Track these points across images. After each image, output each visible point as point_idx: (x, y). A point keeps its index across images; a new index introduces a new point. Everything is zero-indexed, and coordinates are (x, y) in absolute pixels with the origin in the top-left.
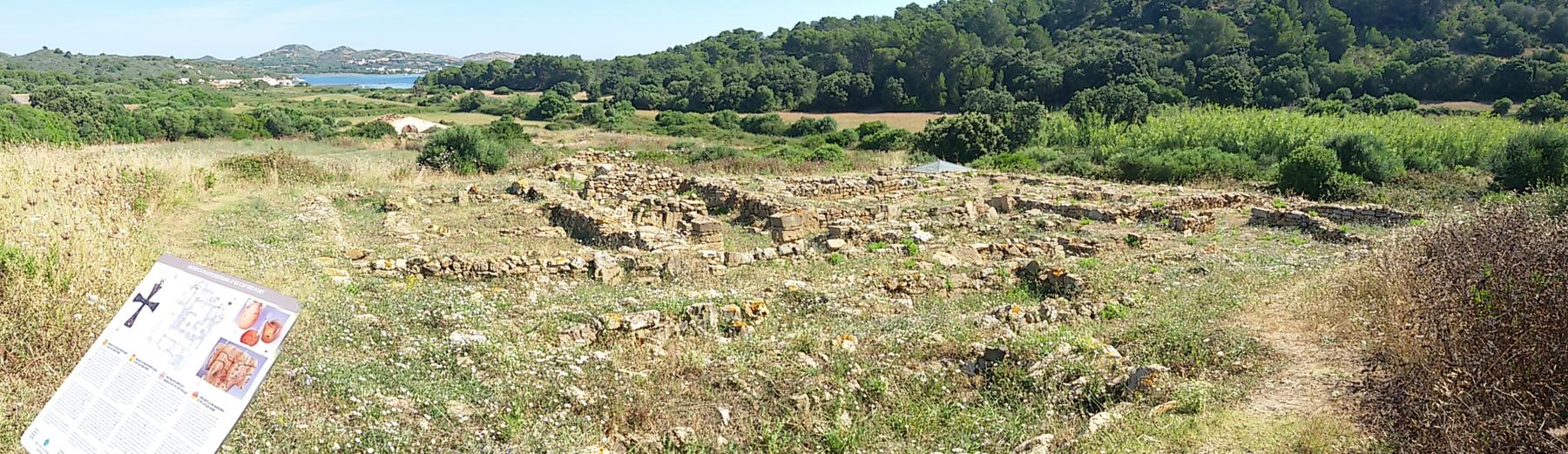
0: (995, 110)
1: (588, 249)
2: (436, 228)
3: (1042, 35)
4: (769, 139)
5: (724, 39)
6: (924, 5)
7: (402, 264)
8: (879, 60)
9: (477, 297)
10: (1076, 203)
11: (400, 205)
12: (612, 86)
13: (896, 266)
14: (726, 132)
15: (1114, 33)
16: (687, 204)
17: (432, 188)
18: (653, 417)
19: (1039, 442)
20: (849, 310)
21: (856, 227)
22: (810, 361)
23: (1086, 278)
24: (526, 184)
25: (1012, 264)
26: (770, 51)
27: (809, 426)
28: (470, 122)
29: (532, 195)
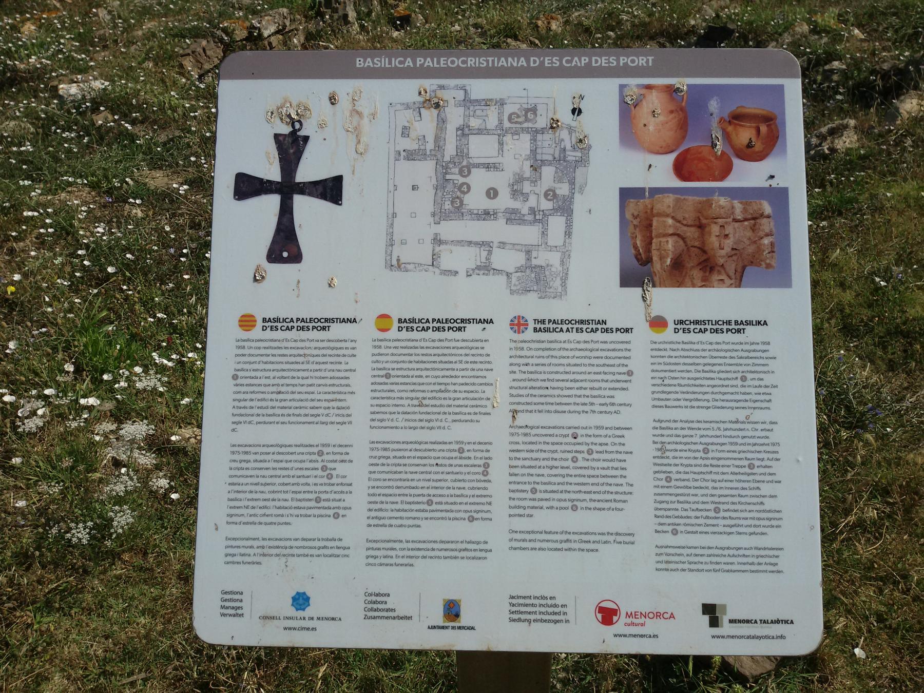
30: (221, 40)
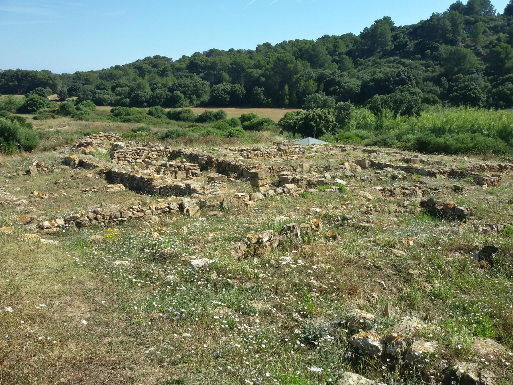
3: (348, 62)
6: (273, 44)
8: (249, 76)
14: (158, 120)
15: (395, 60)
26: (179, 70)
30: (246, 243)
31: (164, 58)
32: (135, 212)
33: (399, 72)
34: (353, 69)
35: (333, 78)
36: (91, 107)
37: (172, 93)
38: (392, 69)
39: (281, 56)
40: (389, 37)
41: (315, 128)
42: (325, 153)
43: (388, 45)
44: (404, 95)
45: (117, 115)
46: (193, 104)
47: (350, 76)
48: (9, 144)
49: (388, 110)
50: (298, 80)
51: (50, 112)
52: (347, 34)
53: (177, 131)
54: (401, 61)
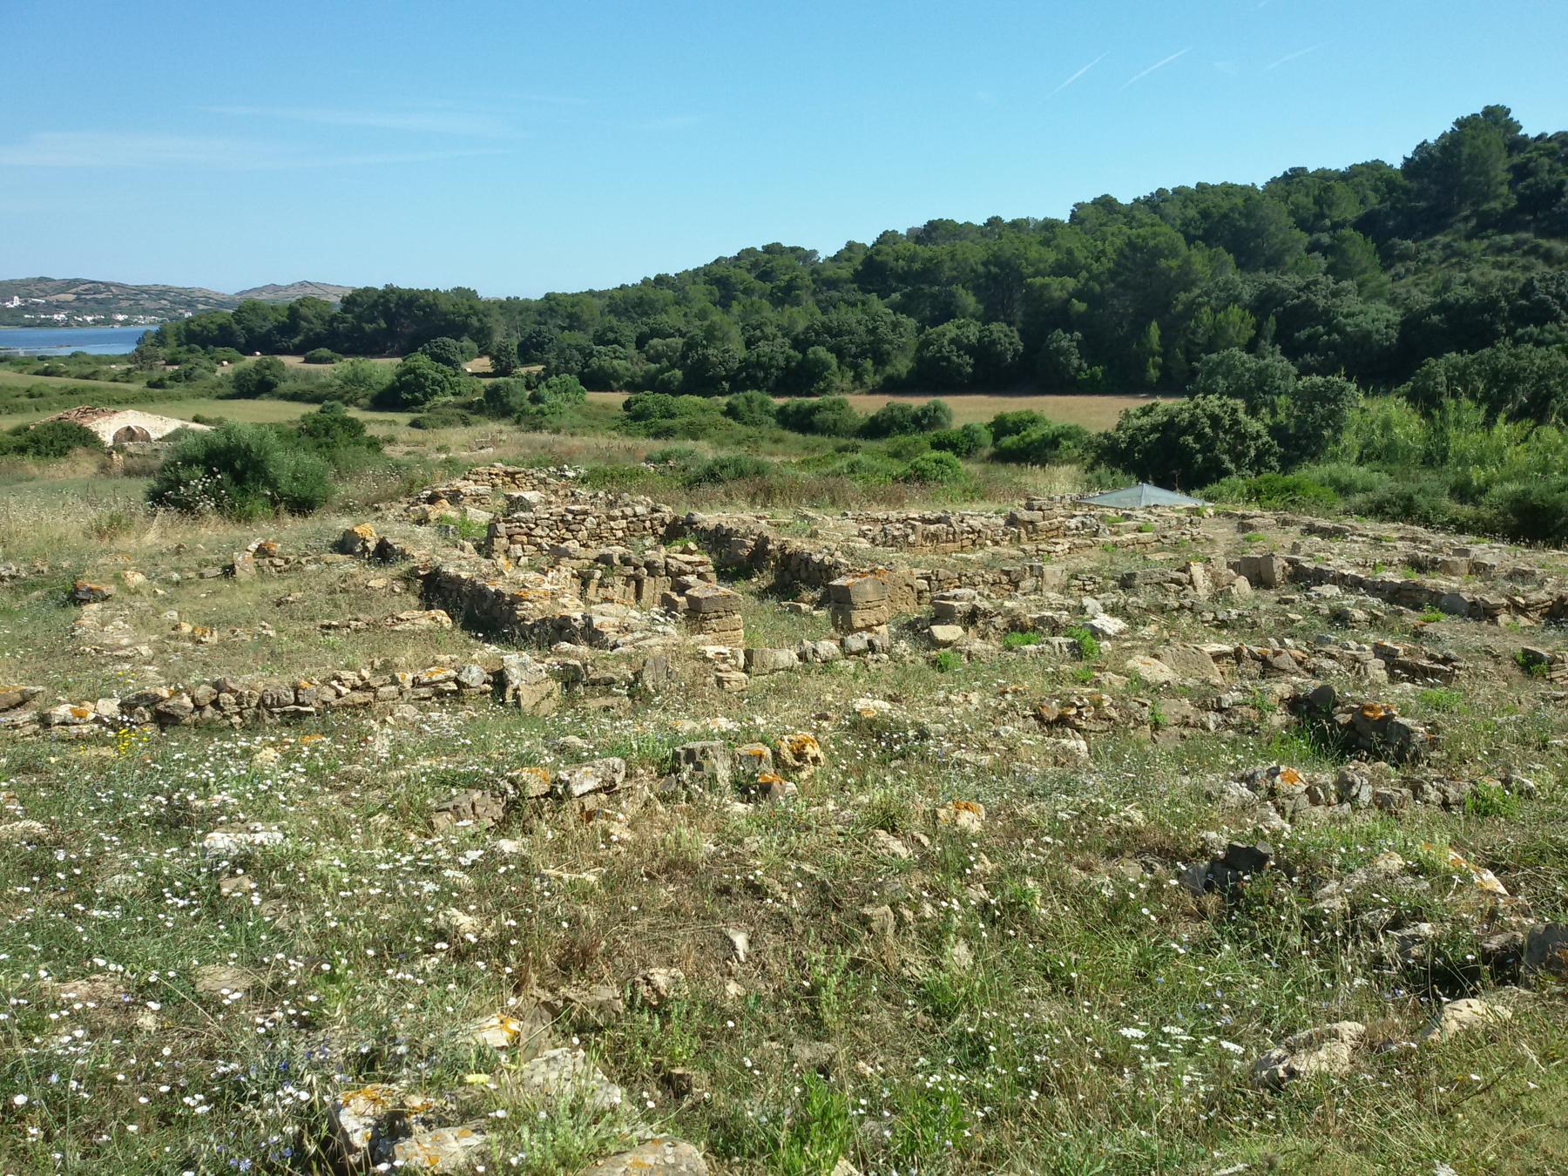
0: (1255, 391)
1: (492, 649)
2: (187, 628)
3: (1361, 249)
4: (828, 443)
5: (745, 263)
6: (1125, 198)
7: (109, 707)
8: (1036, 298)
9: (268, 756)
10: (1416, 578)
11: (110, 589)
12: (540, 346)
13: (1056, 678)
14: (751, 430)
15: (1518, 244)
16: (679, 559)
17: (178, 551)
18: (607, 955)
19: (1335, 1035)
20: (970, 757)
21: (984, 605)
22: (897, 846)
23: (1434, 728)
24: (369, 531)
25: (1281, 689)
26: (832, 284)
27: (894, 962)
28: (251, 417)
29: (384, 553)
31: (793, 250)
32: (344, 691)
33: (1530, 281)
34: (1377, 273)
35: (1308, 300)
36: (571, 396)
37: (804, 352)
38: (1508, 273)
39: (1139, 236)
40: (1500, 170)
41: (1199, 458)
42: (1169, 533)
43: (1498, 197)
44: (1525, 354)
45: (637, 417)
46: (863, 384)
47: (1366, 293)
48: (245, 492)
49: (1467, 403)
50: (1192, 309)
51: (457, 406)
52: (1366, 165)
53: (736, 461)
54: (1538, 246)
